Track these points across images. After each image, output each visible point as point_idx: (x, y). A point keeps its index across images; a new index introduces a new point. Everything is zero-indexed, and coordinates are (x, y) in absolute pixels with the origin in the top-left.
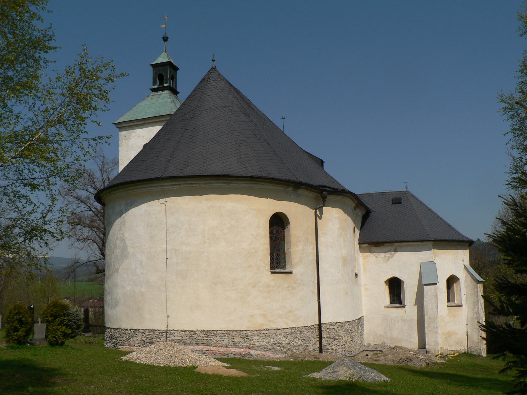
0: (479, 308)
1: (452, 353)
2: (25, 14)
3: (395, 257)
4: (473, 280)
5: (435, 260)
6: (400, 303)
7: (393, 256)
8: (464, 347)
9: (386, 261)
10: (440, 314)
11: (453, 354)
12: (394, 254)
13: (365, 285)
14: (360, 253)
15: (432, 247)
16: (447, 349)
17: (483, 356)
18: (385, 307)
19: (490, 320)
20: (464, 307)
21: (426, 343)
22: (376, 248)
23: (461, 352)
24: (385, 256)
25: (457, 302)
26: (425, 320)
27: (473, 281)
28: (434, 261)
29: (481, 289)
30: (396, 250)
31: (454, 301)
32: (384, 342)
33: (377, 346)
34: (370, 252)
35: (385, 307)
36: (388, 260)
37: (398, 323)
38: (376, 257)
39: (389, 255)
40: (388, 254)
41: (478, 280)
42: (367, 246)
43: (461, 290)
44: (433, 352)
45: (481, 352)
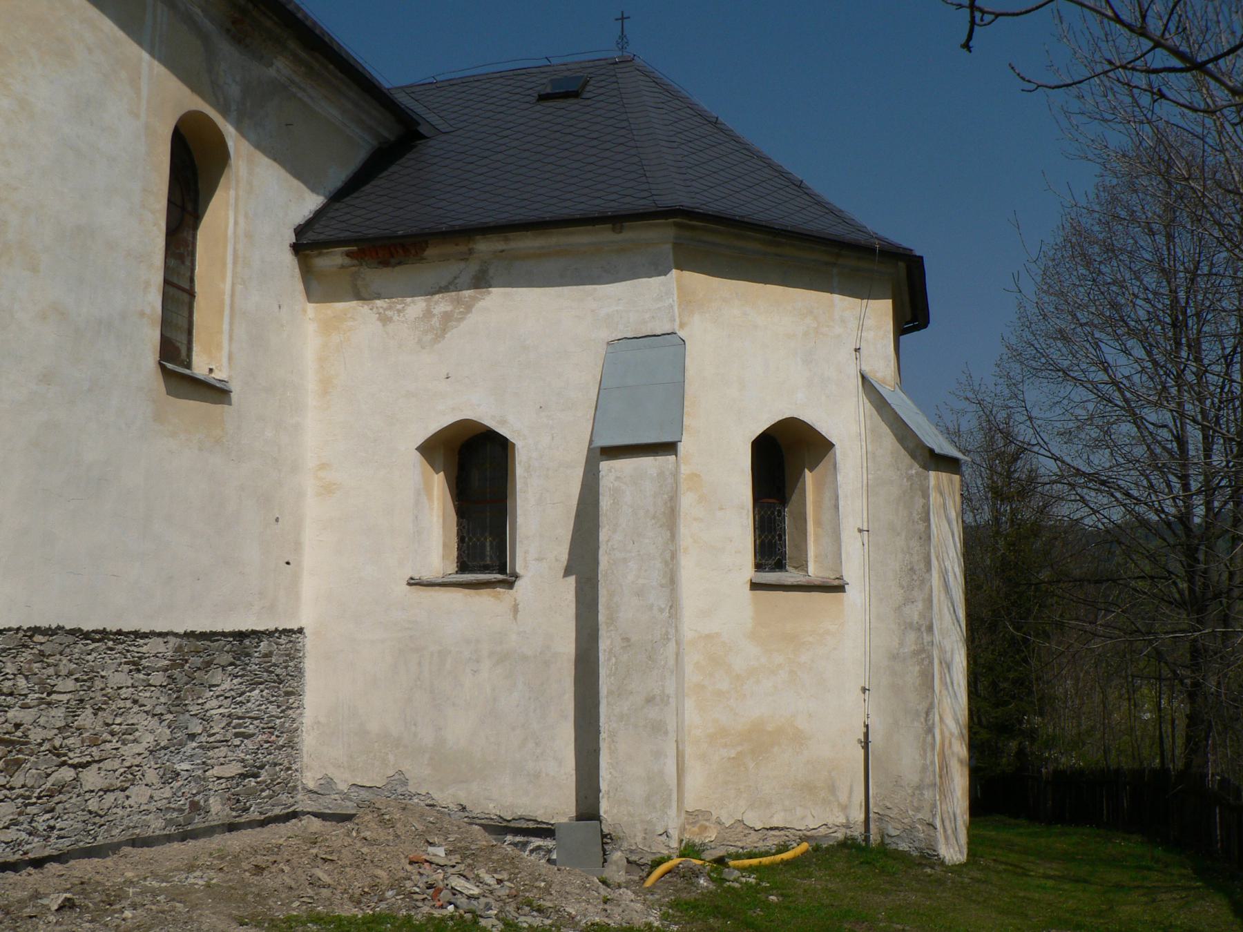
0: (930, 600)
1: (772, 841)
2: (1176, 681)
3: (474, 318)
4: (906, 449)
5: (682, 325)
6: (502, 570)
7: (469, 308)
8: (844, 808)
9: (430, 337)
10: (691, 625)
11: (779, 852)
12: (475, 299)
13: (323, 466)
14: (310, 296)
15: (671, 257)
16: (741, 821)
17: (943, 863)
18: (413, 583)
19: (168, 335)
20: (855, 595)
21: (603, 786)
22: (386, 270)
23: (826, 836)
24: (428, 314)
25: (815, 571)
26: (602, 657)
27: (908, 459)
28: (681, 334)
29: (950, 504)
30: (481, 281)
31: (802, 566)
32: (400, 772)
33: (364, 794)
34: (359, 296)
35: (413, 583)
36: (444, 331)
37: (475, 672)
38: (385, 320)
39: (449, 308)
40: (442, 304)
41: (931, 451)
42: (343, 267)
43: (841, 503)
44: (639, 839)
45: (935, 839)
